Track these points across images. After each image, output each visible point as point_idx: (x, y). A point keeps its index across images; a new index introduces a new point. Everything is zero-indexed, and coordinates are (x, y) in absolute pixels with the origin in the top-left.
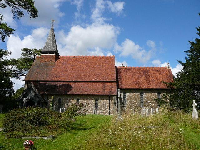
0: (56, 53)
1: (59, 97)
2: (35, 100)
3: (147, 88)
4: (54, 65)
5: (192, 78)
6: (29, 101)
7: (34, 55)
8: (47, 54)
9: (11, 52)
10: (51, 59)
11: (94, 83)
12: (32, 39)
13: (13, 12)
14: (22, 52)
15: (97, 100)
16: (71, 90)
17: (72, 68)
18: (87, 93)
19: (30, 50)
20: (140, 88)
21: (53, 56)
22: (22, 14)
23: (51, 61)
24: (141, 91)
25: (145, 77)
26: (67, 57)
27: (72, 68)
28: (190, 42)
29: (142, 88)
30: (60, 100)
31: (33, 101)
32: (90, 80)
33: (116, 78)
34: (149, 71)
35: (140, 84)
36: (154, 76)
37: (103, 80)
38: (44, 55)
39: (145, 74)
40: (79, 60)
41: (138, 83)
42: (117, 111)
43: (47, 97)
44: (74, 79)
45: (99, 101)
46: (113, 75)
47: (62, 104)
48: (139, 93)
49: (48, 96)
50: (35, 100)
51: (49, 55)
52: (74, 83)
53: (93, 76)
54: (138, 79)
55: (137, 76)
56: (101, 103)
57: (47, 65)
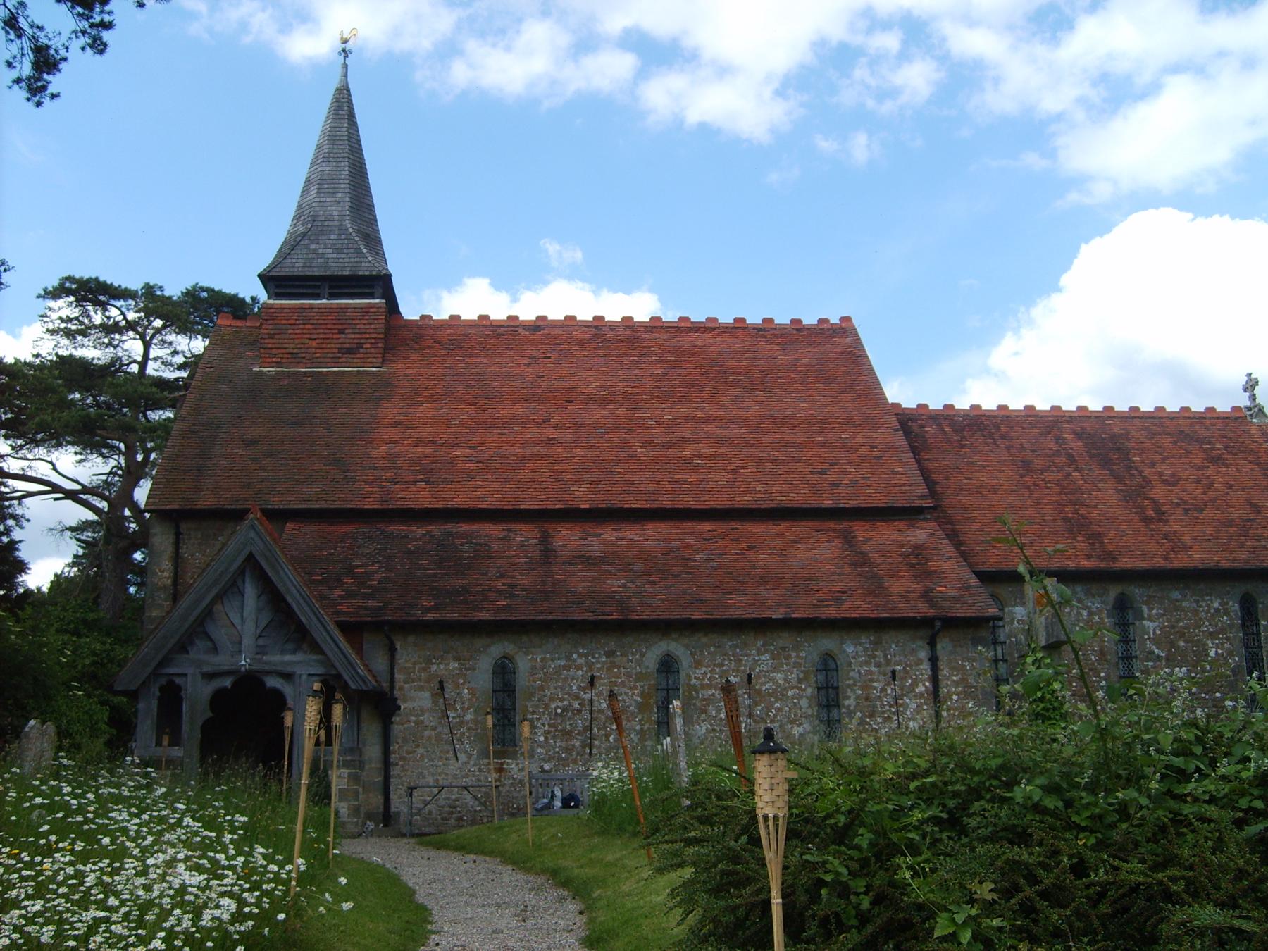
1: (498, 649)
2: (288, 677)
3: (1158, 562)
4: (383, 384)
6: (228, 682)
7: (142, 337)
8: (317, 296)
10: (350, 337)
11: (758, 530)
15: (932, 644)
18: (738, 607)
21: (365, 311)
23: (350, 351)
24: (1113, 592)
26: (471, 325)
28: (39, 296)
29: (1126, 563)
30: (504, 673)
31: (272, 682)
32: (722, 501)
37: (827, 503)
39: (1106, 463)
43: (392, 651)
44: (583, 496)
45: (943, 646)
47: (836, 658)
50: (288, 677)
51: (326, 307)
53: (734, 472)
55: (1051, 476)
56: (866, 687)
57: (324, 387)
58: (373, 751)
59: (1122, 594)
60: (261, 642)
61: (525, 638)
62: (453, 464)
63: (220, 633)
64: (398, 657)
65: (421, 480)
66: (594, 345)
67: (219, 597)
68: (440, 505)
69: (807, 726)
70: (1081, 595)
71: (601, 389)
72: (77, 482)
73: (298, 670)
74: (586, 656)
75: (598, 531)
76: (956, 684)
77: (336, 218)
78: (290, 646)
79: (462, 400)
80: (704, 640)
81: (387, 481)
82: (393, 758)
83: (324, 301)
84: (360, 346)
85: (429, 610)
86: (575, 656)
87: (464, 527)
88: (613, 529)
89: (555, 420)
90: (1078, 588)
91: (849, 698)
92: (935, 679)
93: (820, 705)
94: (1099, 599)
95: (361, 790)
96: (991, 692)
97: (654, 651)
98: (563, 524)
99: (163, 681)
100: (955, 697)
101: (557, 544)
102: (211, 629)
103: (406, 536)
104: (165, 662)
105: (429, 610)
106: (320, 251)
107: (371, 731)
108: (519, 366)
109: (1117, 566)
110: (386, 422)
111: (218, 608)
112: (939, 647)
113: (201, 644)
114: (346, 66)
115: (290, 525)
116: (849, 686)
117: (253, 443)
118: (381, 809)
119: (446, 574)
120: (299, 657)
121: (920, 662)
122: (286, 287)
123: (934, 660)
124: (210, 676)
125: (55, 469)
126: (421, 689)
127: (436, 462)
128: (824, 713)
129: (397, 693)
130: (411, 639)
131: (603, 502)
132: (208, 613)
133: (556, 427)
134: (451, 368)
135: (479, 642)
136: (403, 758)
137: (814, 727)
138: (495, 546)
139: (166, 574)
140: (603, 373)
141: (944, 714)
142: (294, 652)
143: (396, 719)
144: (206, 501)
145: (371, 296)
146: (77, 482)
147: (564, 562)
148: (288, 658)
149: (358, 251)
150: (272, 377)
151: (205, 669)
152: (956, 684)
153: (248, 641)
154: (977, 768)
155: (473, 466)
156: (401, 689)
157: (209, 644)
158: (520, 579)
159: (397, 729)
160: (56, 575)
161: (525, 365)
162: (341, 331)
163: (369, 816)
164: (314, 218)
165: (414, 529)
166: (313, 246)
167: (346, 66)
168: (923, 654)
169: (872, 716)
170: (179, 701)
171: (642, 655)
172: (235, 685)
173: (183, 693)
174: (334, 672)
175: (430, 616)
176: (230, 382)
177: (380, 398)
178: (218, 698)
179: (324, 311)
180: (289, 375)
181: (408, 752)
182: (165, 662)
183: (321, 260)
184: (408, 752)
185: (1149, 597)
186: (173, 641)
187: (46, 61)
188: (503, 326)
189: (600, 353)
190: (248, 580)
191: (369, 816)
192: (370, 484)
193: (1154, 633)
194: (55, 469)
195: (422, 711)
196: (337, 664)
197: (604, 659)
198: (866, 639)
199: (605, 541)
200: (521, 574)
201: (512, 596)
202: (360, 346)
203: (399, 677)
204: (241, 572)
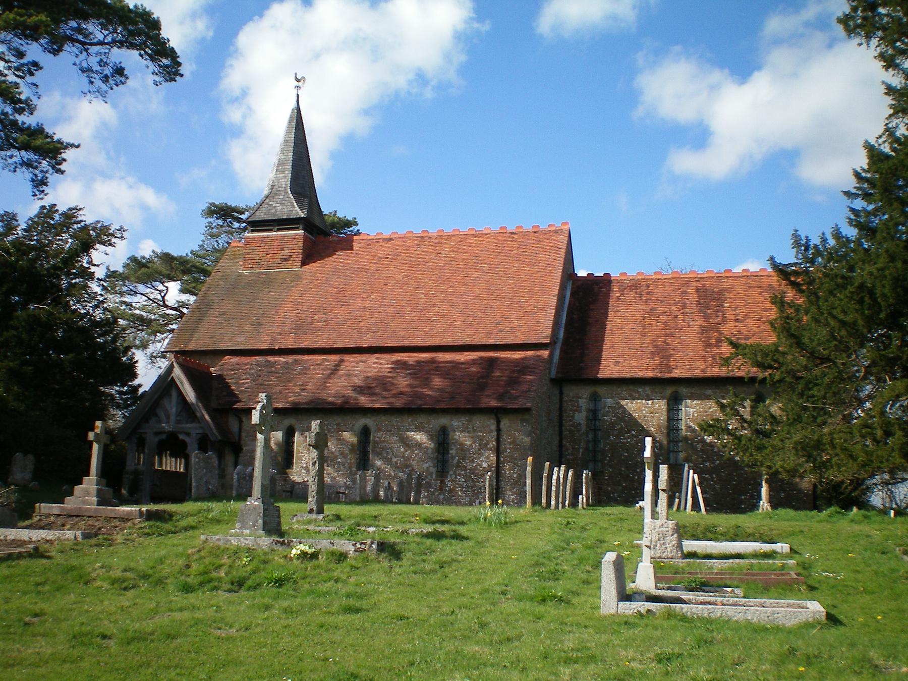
2: (188, 434)
3: (698, 373)
6: (164, 437)
8: (270, 230)
9: (121, 229)
12: (874, 42)
13: (83, 71)
14: (205, 221)
20: (667, 376)
22: (119, 71)
23: (286, 260)
24: (669, 391)
25: (700, 322)
26: (403, 238)
29: (677, 373)
30: (365, 433)
31: (181, 437)
33: (549, 332)
34: (728, 290)
35: (671, 355)
36: (746, 317)
41: (662, 352)
46: (540, 315)
48: (663, 398)
50: (188, 434)
54: (670, 330)
59: (676, 392)
60: (178, 418)
61: (300, 417)
69: (430, 463)
70: (649, 392)
76: (510, 443)
77: (284, 186)
80: (383, 418)
83: (275, 233)
90: (647, 388)
91: (452, 449)
92: (498, 440)
93: (439, 453)
94: (659, 395)
97: (362, 421)
100: (508, 451)
109: (672, 375)
112: (502, 424)
113: (154, 419)
114: (298, 95)
116: (453, 443)
121: (492, 431)
122: (258, 226)
123: (499, 430)
124: (157, 434)
128: (440, 457)
129: (242, 442)
137: (434, 464)
141: (502, 459)
143: (241, 455)
145: (297, 229)
148: (188, 425)
149: (292, 204)
152: (510, 443)
153: (173, 418)
154: (855, 509)
162: (282, 249)
164: (273, 187)
166: (270, 203)
167: (298, 95)
168: (493, 427)
169: (464, 459)
171: (353, 425)
183: (273, 211)
185: (692, 393)
192: (268, 335)
193: (693, 415)
198: (464, 419)
199: (368, 365)
203: (243, 434)
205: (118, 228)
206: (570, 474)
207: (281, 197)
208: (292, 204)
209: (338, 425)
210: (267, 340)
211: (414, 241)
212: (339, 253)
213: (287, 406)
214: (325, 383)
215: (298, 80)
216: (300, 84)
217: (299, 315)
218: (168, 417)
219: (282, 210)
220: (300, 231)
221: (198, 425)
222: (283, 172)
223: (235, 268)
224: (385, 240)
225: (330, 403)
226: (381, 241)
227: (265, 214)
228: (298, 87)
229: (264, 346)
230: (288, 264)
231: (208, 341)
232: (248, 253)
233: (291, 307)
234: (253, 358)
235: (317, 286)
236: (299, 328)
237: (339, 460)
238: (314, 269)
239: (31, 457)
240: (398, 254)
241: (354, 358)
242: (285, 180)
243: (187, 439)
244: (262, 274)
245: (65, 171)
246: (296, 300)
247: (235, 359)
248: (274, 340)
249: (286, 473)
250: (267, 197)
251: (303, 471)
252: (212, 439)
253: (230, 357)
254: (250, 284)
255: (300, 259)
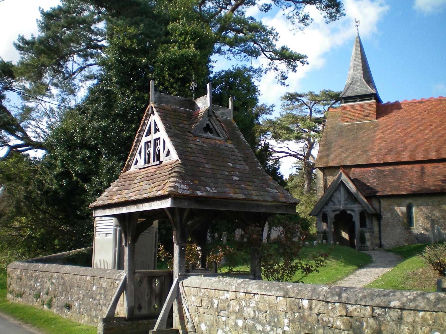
0: (376, 96)
2: (353, 211)
4: (377, 125)
5: (123, 94)
6: (338, 212)
10: (366, 112)
16: (351, 216)
17: (421, 130)
19: (301, 96)
21: (370, 104)
23: (367, 116)
26: (428, 101)
27: (421, 130)
31: (348, 212)
38: (350, 106)
40: (435, 106)
42: (268, 295)
43: (380, 202)
49: (381, 201)
50: (353, 211)
52: (435, 165)
57: (360, 128)
58: (376, 229)
60: (346, 202)
62: (397, 148)
63: (335, 200)
64: (382, 204)
65: (388, 154)
66: (439, 106)
67: (335, 191)
68: (393, 161)
71: (440, 121)
72: (295, 152)
73: (355, 209)
74: (432, 202)
75: (438, 165)
77: (359, 77)
78: (353, 203)
79: (399, 128)
81: (379, 155)
82: (382, 230)
83: (358, 103)
84: (369, 114)
85: (389, 192)
86: (429, 202)
87: (400, 167)
88: (443, 165)
89: (427, 132)
95: (373, 239)
96: (403, 220)
98: (428, 164)
99: (323, 213)
101: (426, 170)
102: (333, 199)
103: (384, 170)
104: (323, 208)
105: (389, 192)
106: (356, 88)
107: (375, 223)
108: (416, 115)
110: (378, 137)
111: (335, 194)
113: (331, 203)
114: (358, 30)
115: (353, 169)
117: (342, 146)
118: (379, 243)
119: (394, 181)
120: (356, 205)
124: (334, 211)
125: (289, 149)
126: (388, 212)
127: (392, 148)
129: (382, 214)
130: (385, 199)
131: (440, 157)
132: (332, 195)
133: (427, 134)
134: (396, 118)
135: (403, 200)
136: (384, 231)
138: (408, 172)
139: (321, 184)
140: (442, 115)
142: (354, 204)
143: (382, 220)
144: (330, 164)
145: (371, 99)
146: (295, 152)
147: (428, 176)
148: (353, 206)
149: (366, 87)
150: (345, 126)
151: (333, 209)
153: (342, 202)
155: (403, 148)
156: (383, 212)
157: (333, 203)
158: (415, 182)
159: (382, 223)
160: (290, 175)
161: (418, 115)
162: (364, 111)
163: (376, 245)
164: (353, 78)
165: (386, 168)
166: (353, 87)
167: (358, 30)
170: (327, 217)
172: (340, 213)
173: (328, 216)
174: (364, 209)
175: (389, 194)
176: (334, 129)
177: (376, 130)
178: (336, 216)
179: (358, 106)
180: (350, 125)
181: (386, 229)
182: (323, 208)
183: (356, 91)
184: (386, 229)
186: (324, 203)
187: (284, 78)
188: (412, 103)
189: (441, 108)
190: (341, 187)
191: (376, 245)
192: (373, 156)
194: (289, 149)
195: (389, 218)
196: (365, 207)
197: (437, 203)
199: (440, 169)
200: (415, 180)
201: (412, 187)
202: (369, 114)
203: (382, 209)
204: (340, 185)
205: (271, 105)
206: (130, 238)
207: (359, 83)
208: (366, 87)
209: (439, 202)
210: (374, 159)
211: (437, 102)
212: (395, 111)
213: (409, 193)
214: (422, 180)
215: (357, 22)
216: (358, 24)
217: (387, 145)
218: (340, 202)
219: (361, 90)
220: (373, 101)
221: (359, 205)
222: (357, 70)
223: (337, 122)
224: (419, 103)
225: (433, 190)
226: (417, 103)
227: (352, 93)
228: (357, 26)
229: (374, 162)
230: (369, 118)
231: (340, 161)
232: (344, 114)
233: (381, 140)
234: (369, 169)
235: (390, 129)
236: (390, 151)
237: (441, 221)
238: (384, 120)
239: (240, 229)
240: (431, 109)
241: (429, 165)
242: (360, 74)
243: (352, 213)
244: (355, 124)
245: (296, 71)
246: (381, 137)
247: (358, 170)
248: (378, 159)
249: (410, 229)
250: (351, 84)
251: (420, 228)
252: (369, 212)
253: (355, 169)
254: (350, 131)
255: (376, 115)
